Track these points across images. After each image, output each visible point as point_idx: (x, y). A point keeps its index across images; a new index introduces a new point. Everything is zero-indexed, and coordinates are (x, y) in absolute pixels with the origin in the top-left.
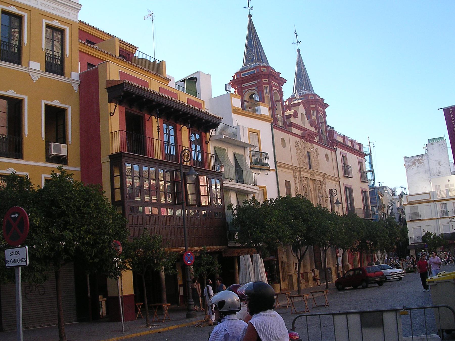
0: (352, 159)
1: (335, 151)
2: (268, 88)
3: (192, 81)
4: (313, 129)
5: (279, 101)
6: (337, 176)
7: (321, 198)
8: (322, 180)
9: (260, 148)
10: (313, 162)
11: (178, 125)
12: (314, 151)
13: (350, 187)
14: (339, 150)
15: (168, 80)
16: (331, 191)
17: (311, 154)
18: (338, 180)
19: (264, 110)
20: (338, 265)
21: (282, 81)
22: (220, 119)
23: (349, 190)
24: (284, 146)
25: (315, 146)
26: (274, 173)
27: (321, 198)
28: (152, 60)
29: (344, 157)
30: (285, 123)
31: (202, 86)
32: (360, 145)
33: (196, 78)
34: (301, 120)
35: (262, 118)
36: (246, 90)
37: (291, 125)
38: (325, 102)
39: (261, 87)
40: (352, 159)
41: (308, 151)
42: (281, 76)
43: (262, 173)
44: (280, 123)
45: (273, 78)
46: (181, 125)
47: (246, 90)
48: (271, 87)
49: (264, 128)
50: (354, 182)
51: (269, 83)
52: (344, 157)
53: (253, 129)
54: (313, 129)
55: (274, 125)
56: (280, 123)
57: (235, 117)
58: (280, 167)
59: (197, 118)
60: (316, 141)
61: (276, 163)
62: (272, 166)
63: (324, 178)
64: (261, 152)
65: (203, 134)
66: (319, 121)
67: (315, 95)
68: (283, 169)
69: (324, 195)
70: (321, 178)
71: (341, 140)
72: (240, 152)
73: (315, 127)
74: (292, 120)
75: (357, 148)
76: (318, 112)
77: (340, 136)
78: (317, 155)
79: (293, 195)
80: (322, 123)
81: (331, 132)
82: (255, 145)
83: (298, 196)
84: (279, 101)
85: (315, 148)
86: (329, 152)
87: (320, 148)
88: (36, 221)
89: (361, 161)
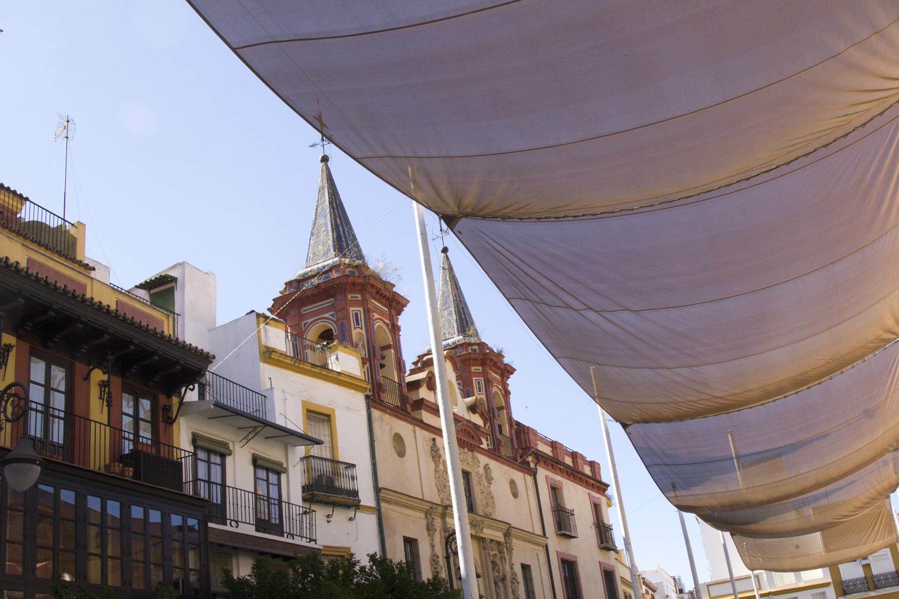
0: (576, 497)
1: (534, 474)
2: (362, 316)
3: (162, 288)
4: (477, 419)
5: (388, 347)
6: (539, 531)
7: (500, 584)
8: (502, 540)
9: (333, 448)
10: (479, 498)
11: (80, 368)
12: (482, 471)
13: (572, 559)
14: (543, 473)
15: (89, 268)
16: (525, 568)
17: (474, 479)
18: (542, 540)
19: (346, 361)
20: (450, 538)
21: (398, 303)
22: (206, 359)
23: (569, 567)
24: (401, 453)
25: (483, 459)
26: (372, 519)
27: (500, 584)
28: (54, 223)
29: (555, 490)
30: (403, 399)
31: (187, 298)
32: (593, 465)
33: (174, 280)
34: (448, 400)
35: (342, 380)
36: (310, 321)
37: (420, 404)
38: (506, 360)
39: (345, 310)
40: (576, 497)
41: (468, 469)
42: (395, 290)
43: (340, 516)
44: (391, 398)
45: (374, 290)
46: (89, 365)
47: (310, 321)
48: (367, 312)
49: (350, 410)
50: (584, 548)
51: (363, 303)
52: (555, 490)
53: (317, 398)
54: (477, 419)
55: (374, 400)
56: (391, 398)
57: (268, 371)
58: (389, 502)
59: (132, 347)
60: (484, 446)
61: (377, 490)
62: (367, 497)
63: (507, 534)
64: (335, 462)
65: (163, 399)
66: (494, 409)
67: (482, 345)
68: (398, 509)
69: (508, 576)
70: (499, 536)
71: (547, 450)
72: (272, 452)
73: (482, 416)
74: (423, 393)
75: (587, 470)
76: (488, 382)
77: (544, 440)
78: (489, 480)
79: (426, 574)
80: (501, 408)
81: (522, 432)
82: (322, 438)
83: (436, 581)
84: (388, 347)
85: (482, 465)
86: (518, 476)
87: (494, 465)
88: (157, 576)
89: (597, 502)
